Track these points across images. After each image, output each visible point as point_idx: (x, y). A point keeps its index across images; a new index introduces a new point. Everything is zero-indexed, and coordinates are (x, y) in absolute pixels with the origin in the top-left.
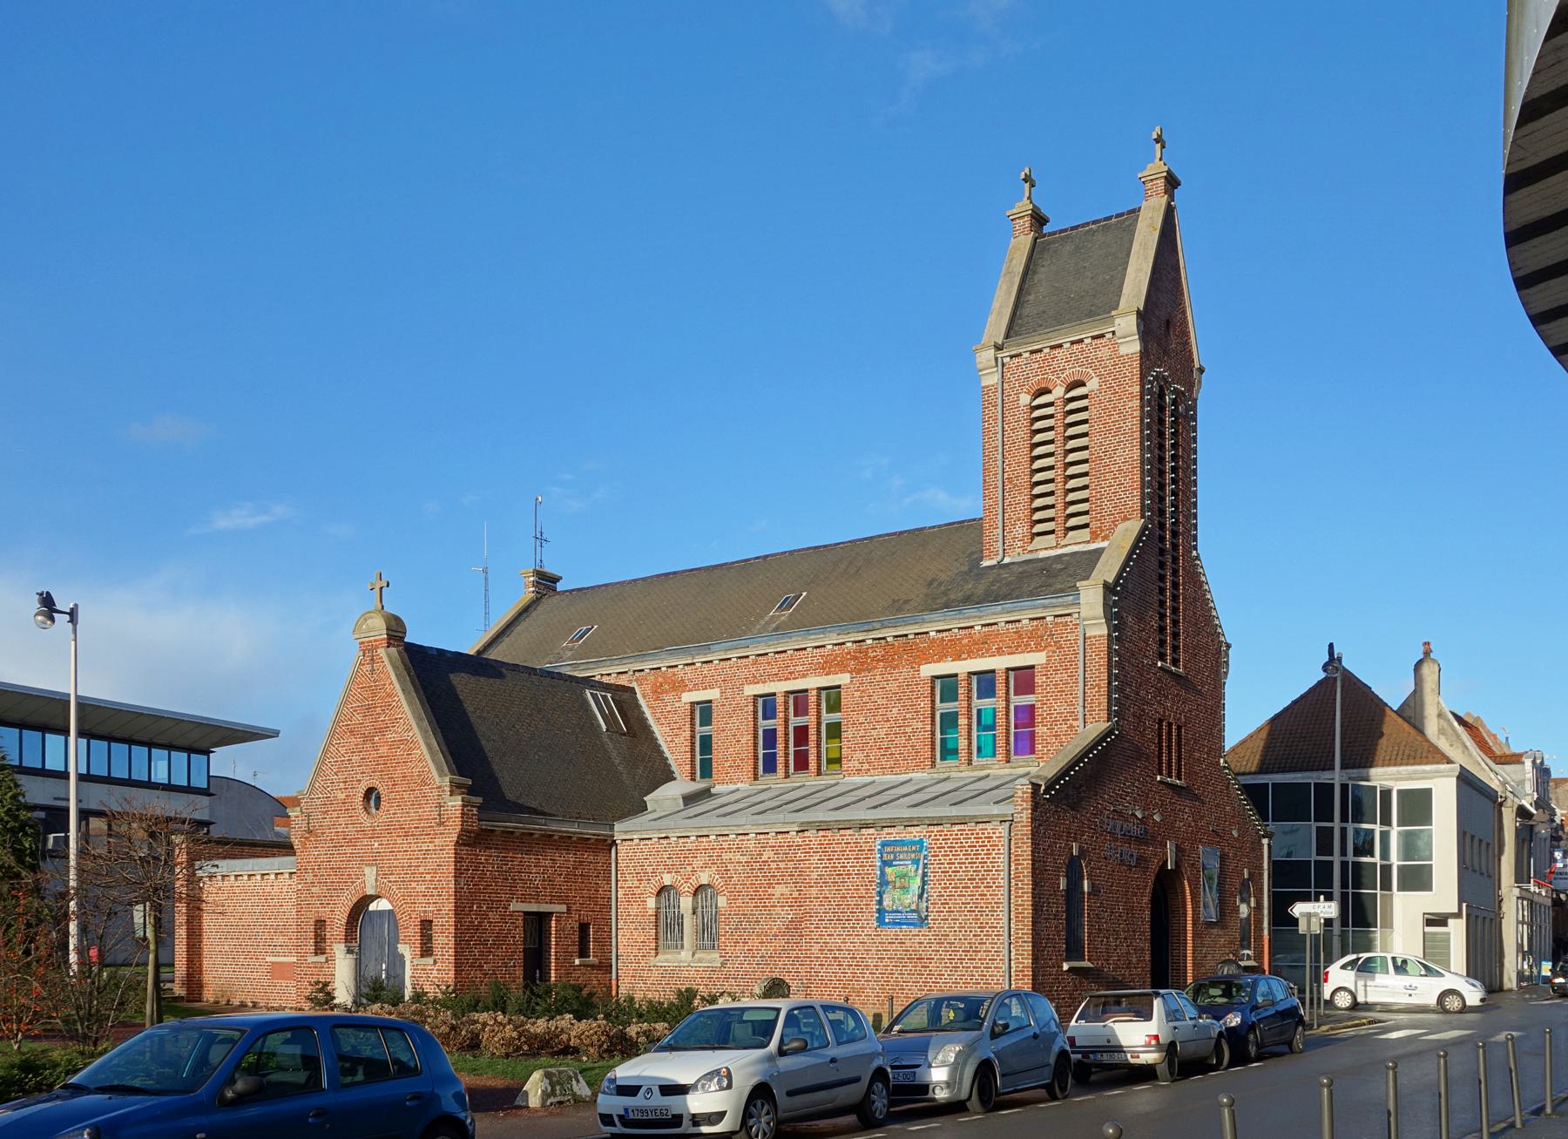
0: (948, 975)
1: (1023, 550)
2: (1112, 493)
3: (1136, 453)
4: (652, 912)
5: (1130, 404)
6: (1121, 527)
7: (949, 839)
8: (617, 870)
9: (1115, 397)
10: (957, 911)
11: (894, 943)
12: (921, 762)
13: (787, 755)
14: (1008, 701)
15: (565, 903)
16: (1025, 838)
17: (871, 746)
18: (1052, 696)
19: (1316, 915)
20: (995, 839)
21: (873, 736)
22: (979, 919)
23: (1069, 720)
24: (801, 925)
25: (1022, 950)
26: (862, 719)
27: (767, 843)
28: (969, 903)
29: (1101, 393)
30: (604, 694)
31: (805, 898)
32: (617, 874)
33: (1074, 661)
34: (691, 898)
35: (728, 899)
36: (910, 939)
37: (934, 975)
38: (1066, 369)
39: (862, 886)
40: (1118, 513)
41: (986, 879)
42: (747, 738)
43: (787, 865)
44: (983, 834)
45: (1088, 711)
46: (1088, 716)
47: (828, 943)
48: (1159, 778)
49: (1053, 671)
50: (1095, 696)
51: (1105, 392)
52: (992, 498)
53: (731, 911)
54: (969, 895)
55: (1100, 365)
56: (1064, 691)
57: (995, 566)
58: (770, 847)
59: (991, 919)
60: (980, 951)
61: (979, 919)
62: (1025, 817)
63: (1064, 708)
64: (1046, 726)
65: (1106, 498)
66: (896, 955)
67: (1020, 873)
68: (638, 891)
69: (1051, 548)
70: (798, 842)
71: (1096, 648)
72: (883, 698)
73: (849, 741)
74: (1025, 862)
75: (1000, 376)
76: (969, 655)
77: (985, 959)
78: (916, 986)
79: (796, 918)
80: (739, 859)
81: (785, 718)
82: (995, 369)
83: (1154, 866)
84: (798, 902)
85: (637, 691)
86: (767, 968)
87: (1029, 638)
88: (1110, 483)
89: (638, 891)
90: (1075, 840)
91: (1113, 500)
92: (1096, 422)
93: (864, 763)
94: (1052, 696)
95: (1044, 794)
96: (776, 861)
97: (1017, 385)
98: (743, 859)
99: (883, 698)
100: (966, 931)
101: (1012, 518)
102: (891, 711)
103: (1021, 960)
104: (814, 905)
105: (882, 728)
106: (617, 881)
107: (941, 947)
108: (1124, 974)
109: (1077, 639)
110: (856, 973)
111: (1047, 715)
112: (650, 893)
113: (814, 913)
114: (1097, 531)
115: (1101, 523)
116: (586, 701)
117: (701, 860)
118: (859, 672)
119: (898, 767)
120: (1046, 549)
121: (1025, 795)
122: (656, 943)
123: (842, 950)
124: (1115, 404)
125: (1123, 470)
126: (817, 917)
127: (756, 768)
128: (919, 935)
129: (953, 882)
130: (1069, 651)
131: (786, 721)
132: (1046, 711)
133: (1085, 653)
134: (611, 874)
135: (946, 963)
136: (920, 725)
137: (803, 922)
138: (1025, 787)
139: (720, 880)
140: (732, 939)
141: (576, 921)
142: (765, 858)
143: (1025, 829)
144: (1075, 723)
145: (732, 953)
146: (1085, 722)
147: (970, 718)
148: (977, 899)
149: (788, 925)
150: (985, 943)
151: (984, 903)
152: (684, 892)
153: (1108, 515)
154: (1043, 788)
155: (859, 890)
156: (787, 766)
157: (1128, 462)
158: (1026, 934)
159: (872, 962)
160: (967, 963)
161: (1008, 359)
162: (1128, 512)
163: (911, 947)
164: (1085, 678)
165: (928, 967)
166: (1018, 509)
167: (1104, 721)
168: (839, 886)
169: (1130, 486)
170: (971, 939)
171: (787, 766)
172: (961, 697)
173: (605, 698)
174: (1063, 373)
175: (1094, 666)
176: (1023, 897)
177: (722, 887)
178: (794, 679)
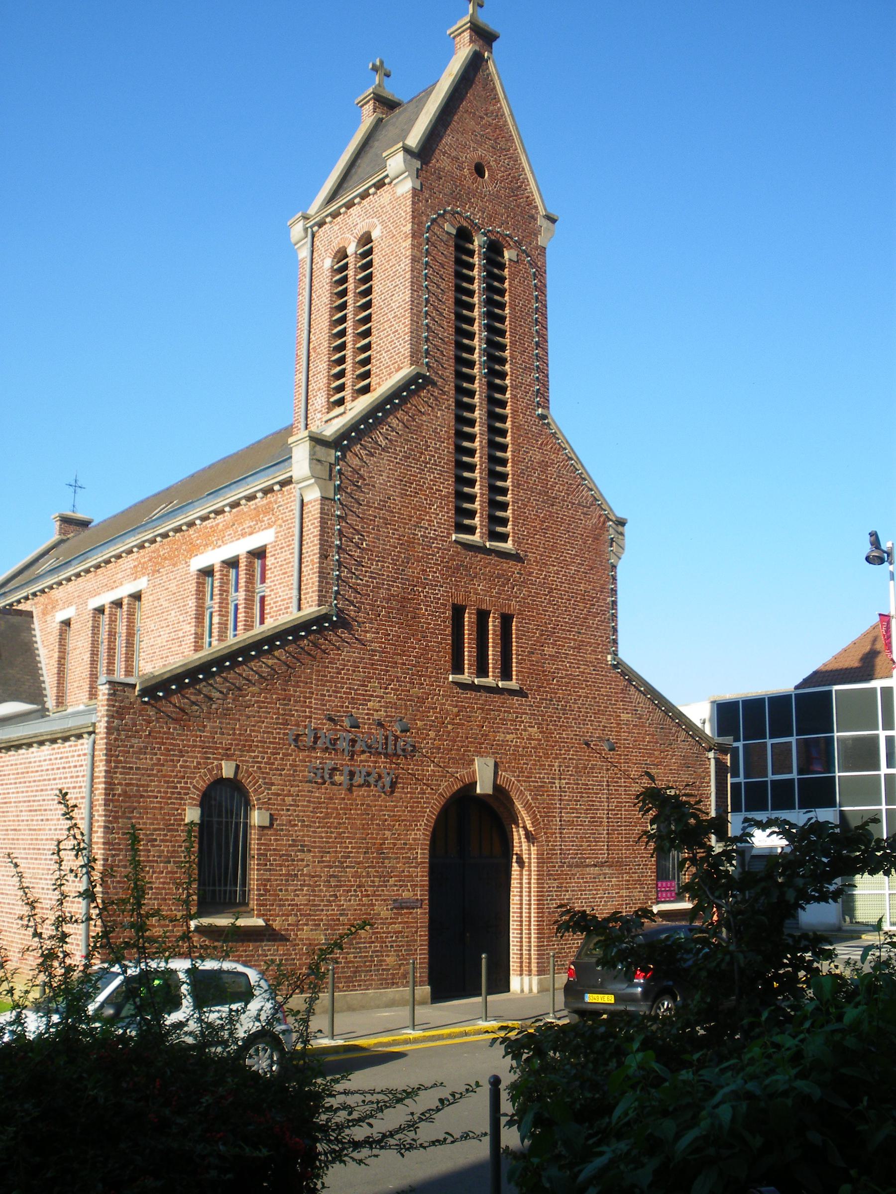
83: (447, 788)
85: (35, 615)
118: (154, 572)
161: (316, 228)
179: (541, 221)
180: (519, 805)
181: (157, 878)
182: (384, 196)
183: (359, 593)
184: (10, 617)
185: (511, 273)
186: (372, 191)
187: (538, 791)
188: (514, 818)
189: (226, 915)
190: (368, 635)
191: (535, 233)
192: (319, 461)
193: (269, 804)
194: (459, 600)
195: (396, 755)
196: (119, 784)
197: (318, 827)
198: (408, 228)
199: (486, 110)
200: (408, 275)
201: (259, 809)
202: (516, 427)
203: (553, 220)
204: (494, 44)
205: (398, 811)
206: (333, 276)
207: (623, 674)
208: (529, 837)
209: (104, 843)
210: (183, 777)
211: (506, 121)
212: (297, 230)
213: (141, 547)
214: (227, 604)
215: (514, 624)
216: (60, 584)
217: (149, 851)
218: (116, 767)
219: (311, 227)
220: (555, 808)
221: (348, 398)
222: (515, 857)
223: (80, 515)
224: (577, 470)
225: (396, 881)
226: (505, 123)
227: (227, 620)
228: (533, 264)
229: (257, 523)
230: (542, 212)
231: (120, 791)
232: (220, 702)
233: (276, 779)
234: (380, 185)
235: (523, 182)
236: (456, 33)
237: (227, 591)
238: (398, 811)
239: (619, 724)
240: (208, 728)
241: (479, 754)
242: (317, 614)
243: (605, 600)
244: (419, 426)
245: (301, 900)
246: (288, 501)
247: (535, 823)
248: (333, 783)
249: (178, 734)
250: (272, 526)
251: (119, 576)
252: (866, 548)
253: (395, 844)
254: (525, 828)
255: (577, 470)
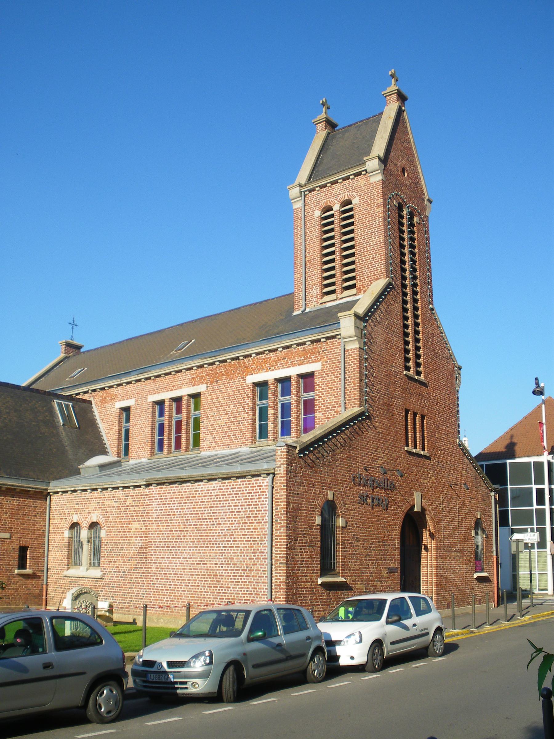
0: (233, 588)
1: (317, 303)
2: (369, 264)
3: (382, 238)
4: (66, 540)
5: (377, 210)
6: (375, 283)
7: (235, 488)
8: (50, 512)
9: (369, 207)
10: (239, 541)
11: (200, 564)
12: (245, 440)
13: (170, 439)
14: (298, 396)
15: (9, 532)
16: (282, 485)
17: (217, 431)
18: (325, 391)
19: (522, 541)
20: (263, 487)
21: (218, 424)
22: (253, 547)
23: (335, 407)
24: (146, 550)
25: (280, 570)
26: (212, 414)
27: (129, 493)
28: (247, 535)
29: (360, 205)
30: (67, 403)
31: (149, 531)
32: (50, 515)
33: (339, 367)
34: (87, 531)
35: (107, 532)
36: (210, 561)
37: (224, 587)
38: (340, 194)
39: (182, 522)
40: (372, 276)
41: (258, 517)
42: (148, 430)
43: (139, 508)
44: (256, 483)
45: (348, 400)
46: (347, 404)
47: (161, 563)
48: (406, 448)
49: (326, 374)
50: (351, 389)
51: (363, 204)
52: (299, 273)
53: (108, 540)
54: (247, 529)
55: (360, 190)
56: (332, 388)
57: (300, 314)
58: (131, 496)
59: (260, 547)
60: (253, 570)
61: (253, 547)
62: (282, 470)
63: (332, 399)
64: (322, 411)
65: (365, 267)
66: (201, 572)
67: (279, 511)
68: (60, 526)
69: (334, 300)
70: (146, 492)
71: (352, 357)
72: (224, 399)
73: (205, 428)
74: (282, 504)
75: (303, 202)
76: (275, 368)
77: (256, 576)
78: (213, 595)
79: (144, 545)
80: (113, 504)
81: (169, 415)
82: (300, 198)
83: (405, 508)
84: (145, 534)
85: (93, 403)
86: (126, 580)
87: (311, 354)
88: (368, 257)
89: (60, 526)
90: (330, 488)
91: (370, 268)
92: (358, 222)
93: (212, 442)
94: (325, 391)
95: (299, 453)
96: (133, 506)
97: (313, 206)
98: (116, 504)
99: (224, 399)
100: (244, 556)
101: (311, 284)
102: (229, 407)
103: (278, 577)
104: (154, 537)
105: (223, 419)
106: (50, 519)
107: (228, 567)
108: (376, 586)
109: (340, 352)
110: (177, 585)
111: (322, 404)
112: (66, 527)
113: (154, 542)
114: (360, 288)
115: (363, 283)
116: (52, 407)
117: (93, 506)
118: (212, 382)
119: (232, 444)
120: (330, 301)
121: (282, 454)
122: (68, 561)
123: (169, 568)
124: (369, 211)
125: (375, 249)
126: (155, 544)
127: (152, 448)
128: (215, 558)
129: (237, 520)
130: (336, 360)
131: (170, 417)
132: (321, 402)
133: (345, 361)
134: (46, 514)
135: (231, 579)
136: (246, 415)
137: (147, 548)
138: (282, 448)
139: (103, 519)
140: (108, 559)
141: (17, 544)
142: (127, 504)
143: (282, 479)
144: (339, 409)
145: (108, 569)
146: (345, 408)
147: (275, 410)
148: (252, 532)
149: (139, 550)
150: (256, 564)
151: (256, 535)
152: (84, 527)
153: (367, 277)
154: (298, 449)
155: (179, 525)
156: (169, 446)
157: (377, 244)
158: (282, 557)
159: (187, 577)
160: (244, 579)
161: (308, 192)
162: (378, 274)
163: (210, 567)
164: (345, 378)
165: (220, 581)
166: (314, 278)
167: (358, 407)
168: (168, 523)
169: (379, 259)
170: (247, 561)
171: (169, 446)
172: (270, 395)
173: (67, 406)
174: (339, 197)
175: (351, 370)
176: (280, 529)
177: (104, 523)
178: (175, 390)
179: (426, 202)
180: (428, 518)
181: (306, 555)
182: (361, 181)
183: (373, 401)
184: (80, 403)
185: (418, 230)
186: (352, 177)
187: (436, 510)
188: (424, 525)
189: (328, 576)
190: (377, 424)
191: (424, 209)
192: (358, 327)
193: (345, 515)
194: (407, 407)
195: (388, 489)
196: (292, 502)
197: (362, 528)
198: (381, 201)
199: (404, 139)
200: (382, 228)
201: (342, 517)
202: (423, 314)
203: (430, 202)
204: (405, 102)
205: (389, 520)
206: (321, 221)
207: (462, 450)
208: (432, 536)
209: (287, 536)
210: (314, 499)
211: (411, 146)
212: (294, 192)
213: (201, 366)
214: (277, 403)
215: (425, 420)
216: (120, 385)
217: (302, 540)
218: (290, 493)
219: (304, 192)
220: (441, 520)
221: (338, 291)
222: (423, 546)
223: (76, 342)
224: (444, 339)
225: (389, 558)
226: (411, 148)
227: (277, 412)
228: (424, 225)
229: (306, 358)
230: (427, 197)
231: (291, 507)
232: (327, 457)
233: (347, 501)
234: (359, 174)
235: (419, 180)
236: (388, 94)
237: (277, 396)
238: (389, 520)
239: (461, 476)
240: (323, 473)
241: (416, 490)
242: (360, 412)
243: (455, 409)
244: (391, 311)
245: (356, 568)
246: (335, 347)
247: (435, 528)
248: (367, 504)
249: (313, 475)
250: (319, 361)
251: (178, 383)
252: (534, 386)
253: (388, 537)
254: (429, 531)
255: (444, 339)
